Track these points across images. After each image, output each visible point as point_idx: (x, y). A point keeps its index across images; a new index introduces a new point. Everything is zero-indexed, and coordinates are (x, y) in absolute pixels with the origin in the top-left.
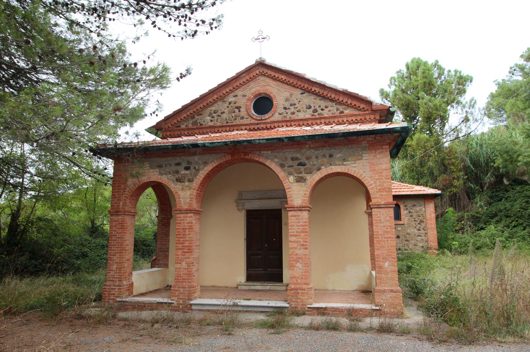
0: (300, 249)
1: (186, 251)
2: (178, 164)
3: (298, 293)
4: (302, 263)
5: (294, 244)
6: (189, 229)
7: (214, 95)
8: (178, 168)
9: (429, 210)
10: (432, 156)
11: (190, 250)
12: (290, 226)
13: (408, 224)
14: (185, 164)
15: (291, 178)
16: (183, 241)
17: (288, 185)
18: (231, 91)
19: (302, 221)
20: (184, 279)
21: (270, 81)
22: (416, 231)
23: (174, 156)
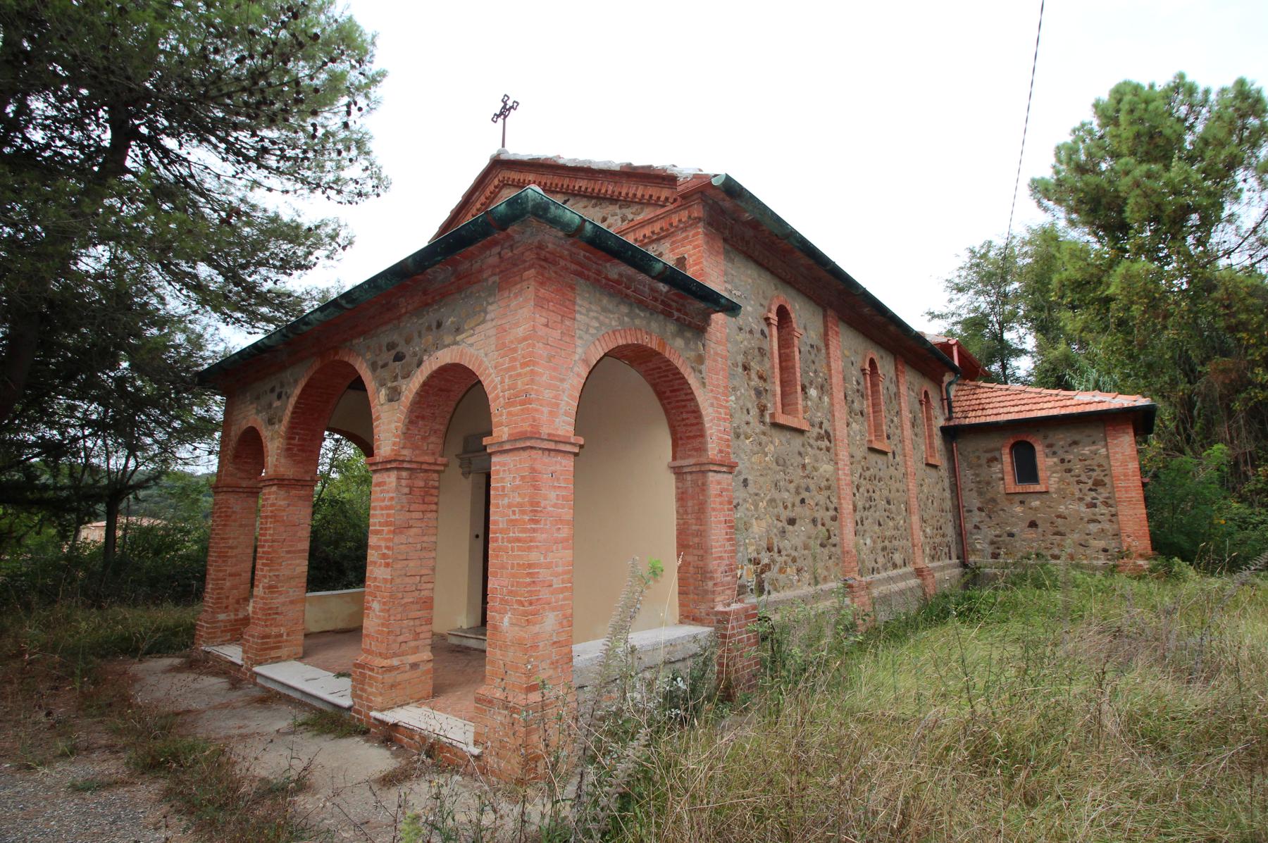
9: (1122, 452)
10: (1172, 314)
13: (1058, 491)
22: (1083, 509)
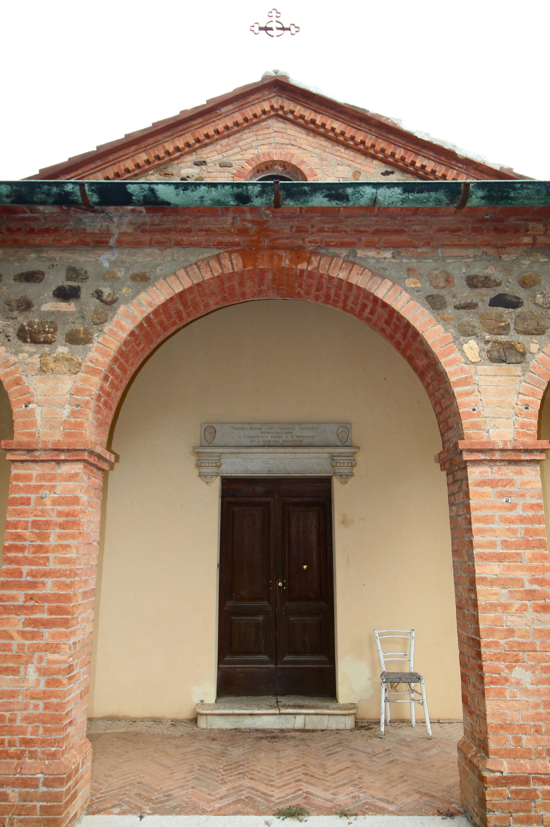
0: (523, 609)
1: (45, 616)
2: (32, 277)
3: (531, 796)
4: (533, 669)
5: (495, 589)
6: (62, 526)
7: (137, 152)
8: (29, 290)
11: (61, 613)
12: (479, 520)
14: (57, 279)
15: (472, 348)
16: (31, 574)
17: (462, 370)
18: (190, 149)
19: (520, 501)
20: (27, 742)
21: (300, 135)
23: (16, 244)
